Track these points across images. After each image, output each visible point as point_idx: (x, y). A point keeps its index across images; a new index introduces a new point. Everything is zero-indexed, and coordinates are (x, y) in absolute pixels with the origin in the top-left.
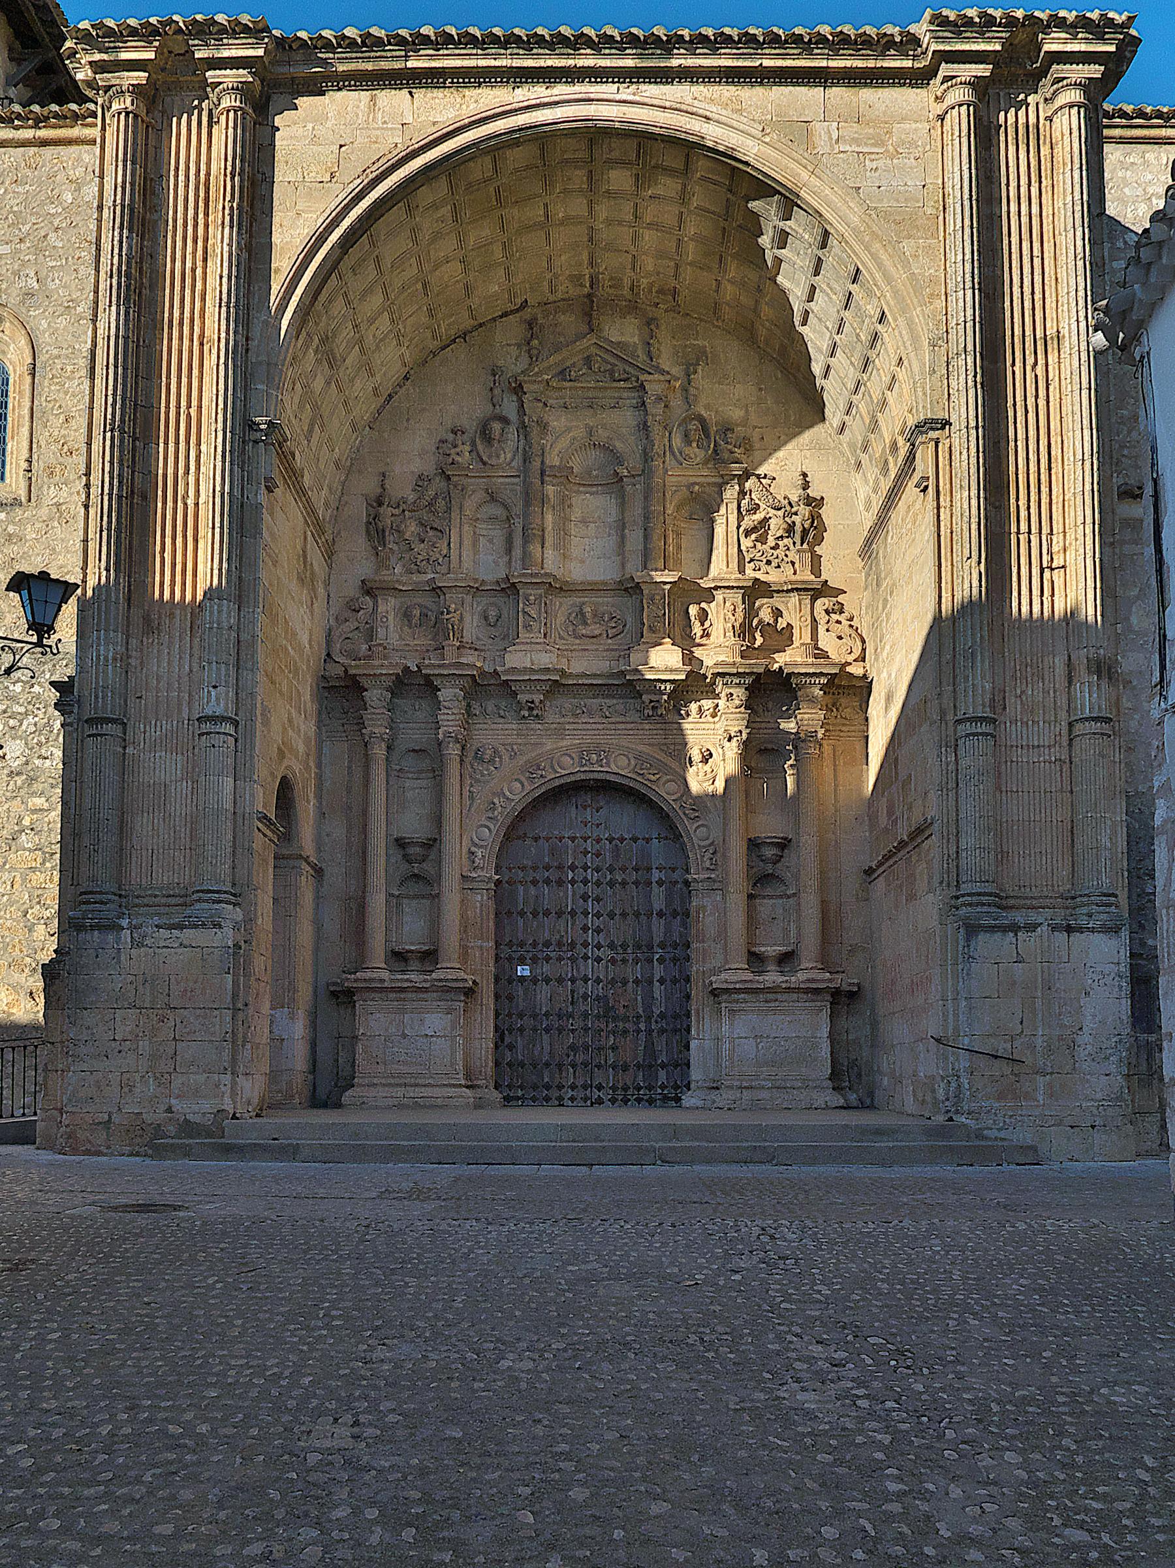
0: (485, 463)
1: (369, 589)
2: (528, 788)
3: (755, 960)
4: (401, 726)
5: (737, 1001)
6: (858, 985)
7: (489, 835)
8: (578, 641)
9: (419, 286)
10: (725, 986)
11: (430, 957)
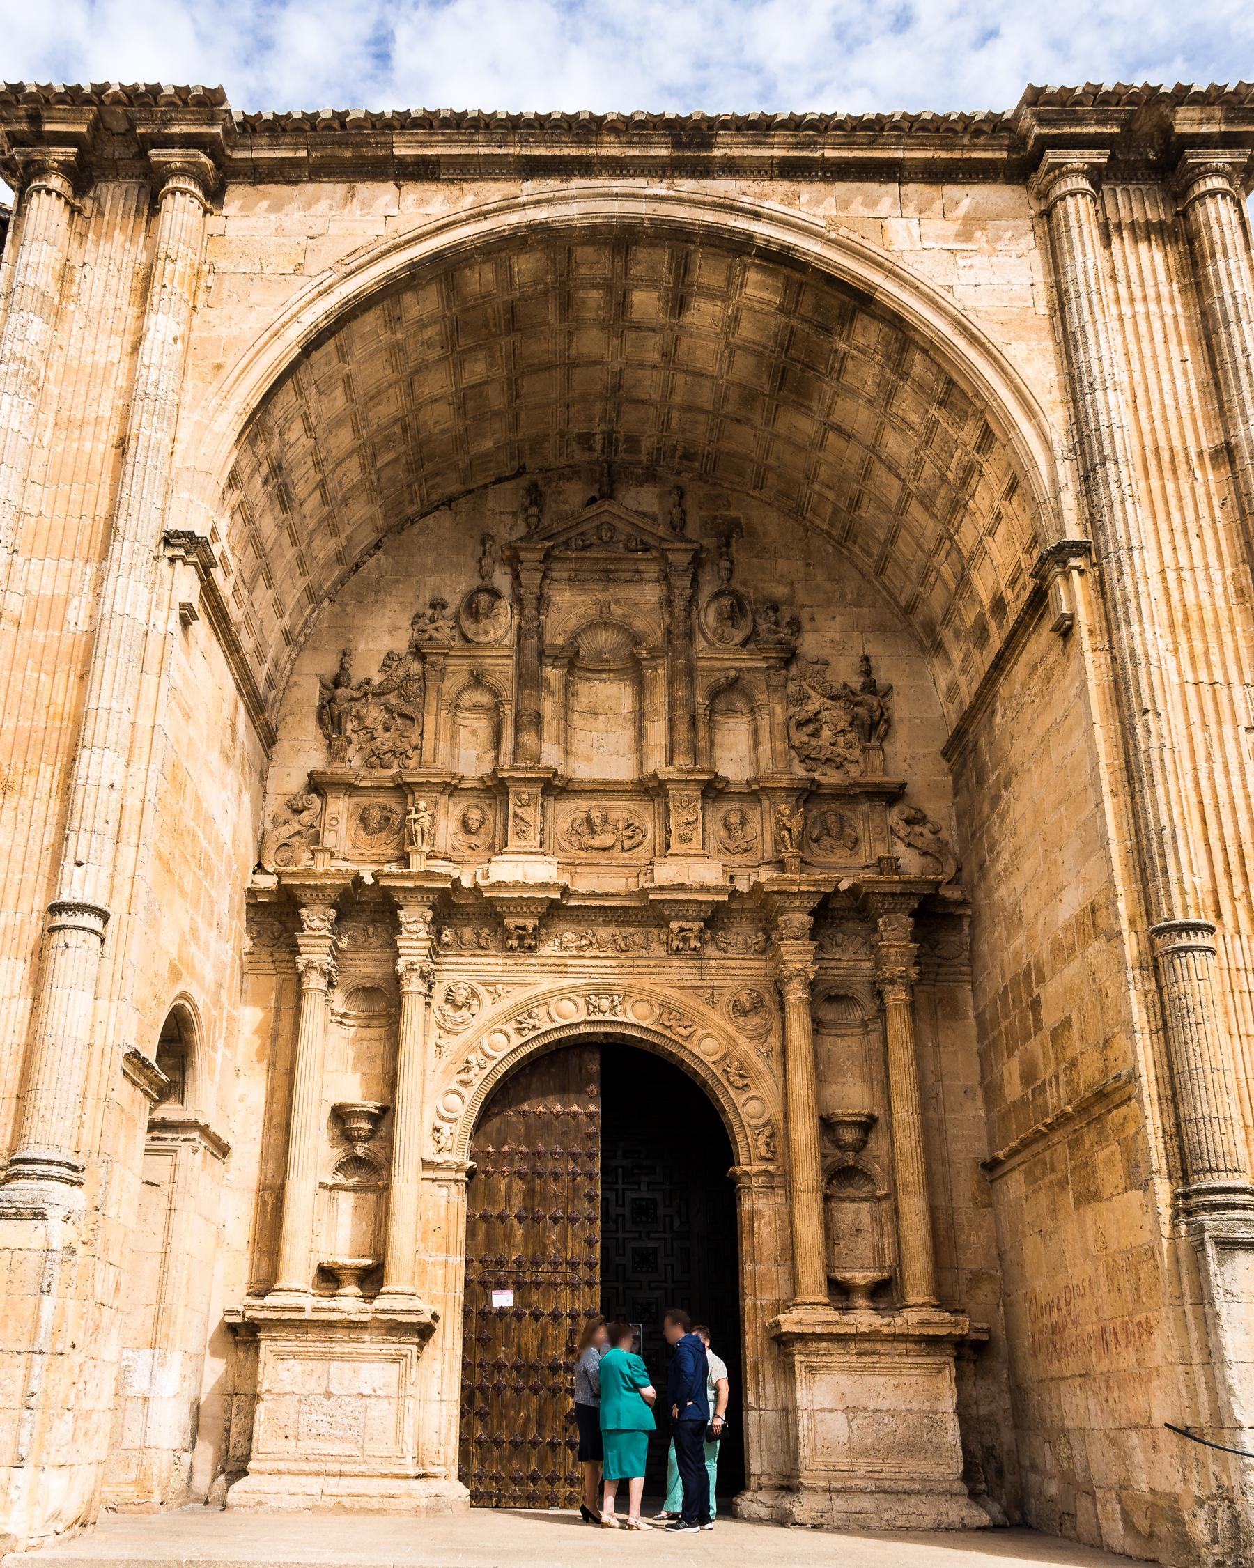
0: (468, 640)
1: (317, 786)
2: (517, 1040)
3: (840, 1292)
4: (349, 956)
5: (817, 1353)
6: (988, 1331)
7: (465, 1107)
8: (583, 854)
9: (397, 429)
10: (798, 1329)
11: (372, 1278)
